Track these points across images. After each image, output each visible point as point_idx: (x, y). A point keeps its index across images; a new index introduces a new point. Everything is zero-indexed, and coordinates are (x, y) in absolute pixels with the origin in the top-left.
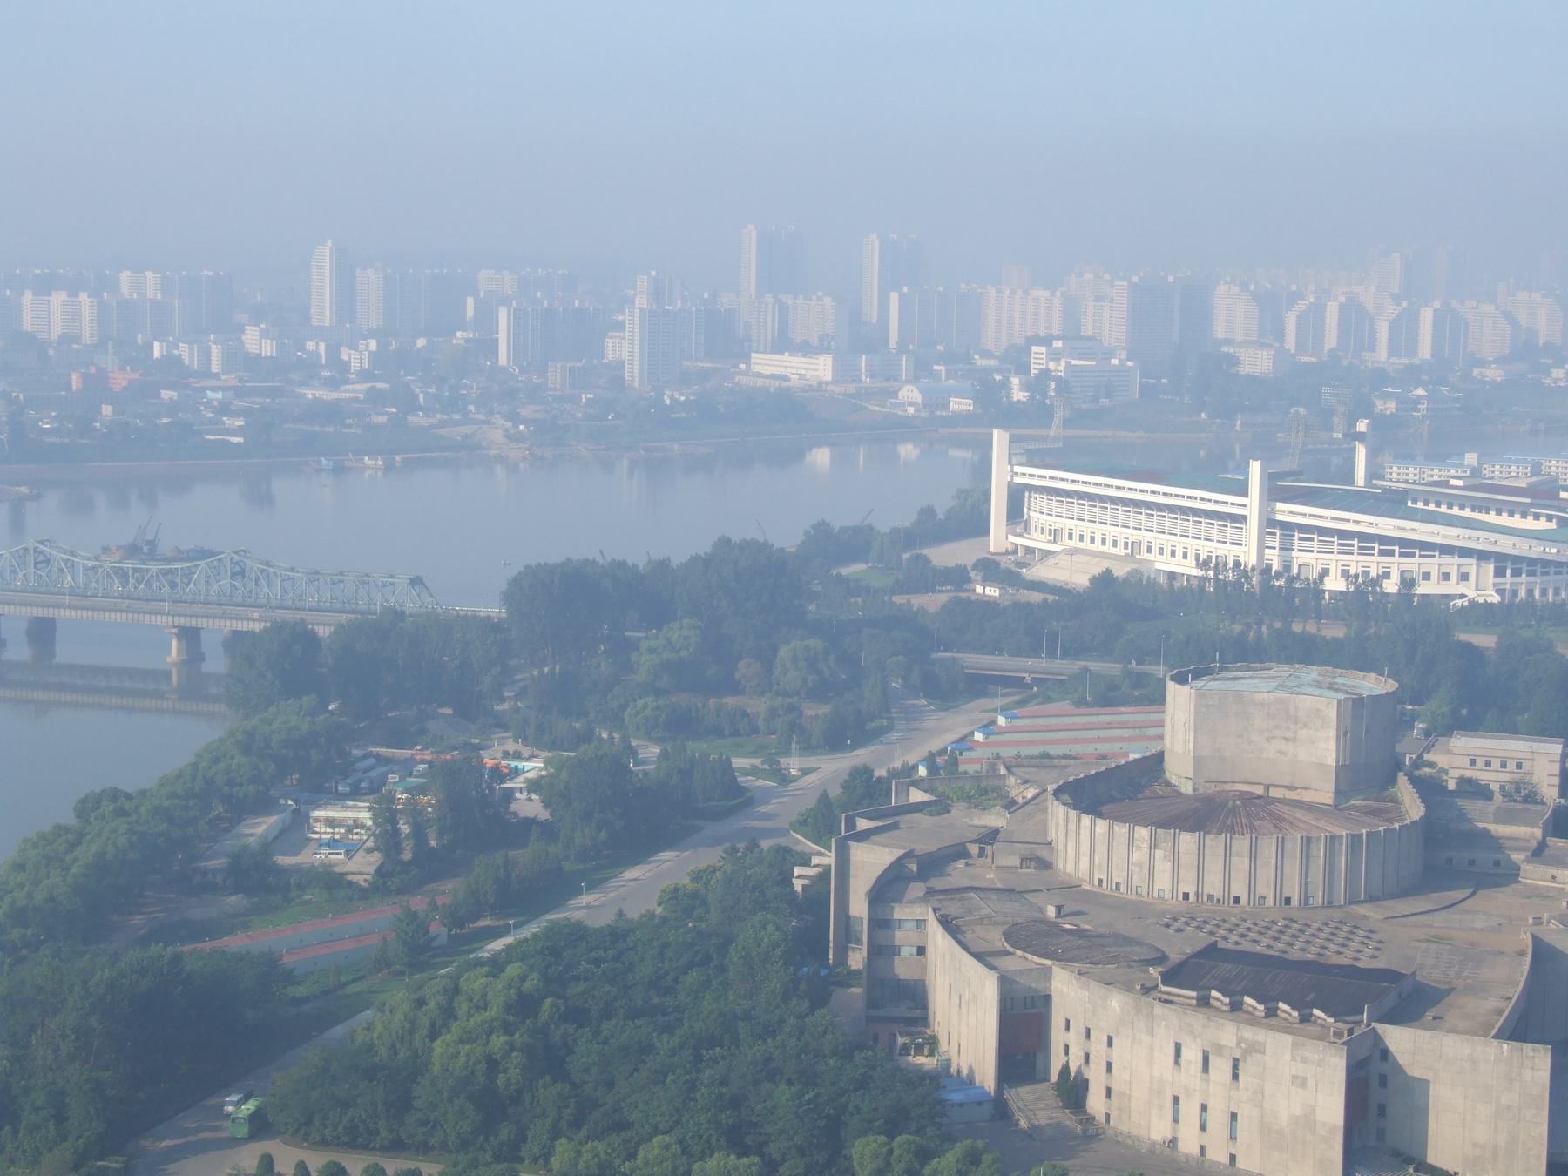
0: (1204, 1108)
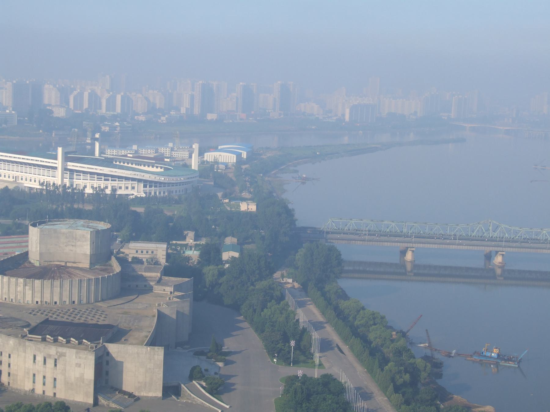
0: (44, 377)
